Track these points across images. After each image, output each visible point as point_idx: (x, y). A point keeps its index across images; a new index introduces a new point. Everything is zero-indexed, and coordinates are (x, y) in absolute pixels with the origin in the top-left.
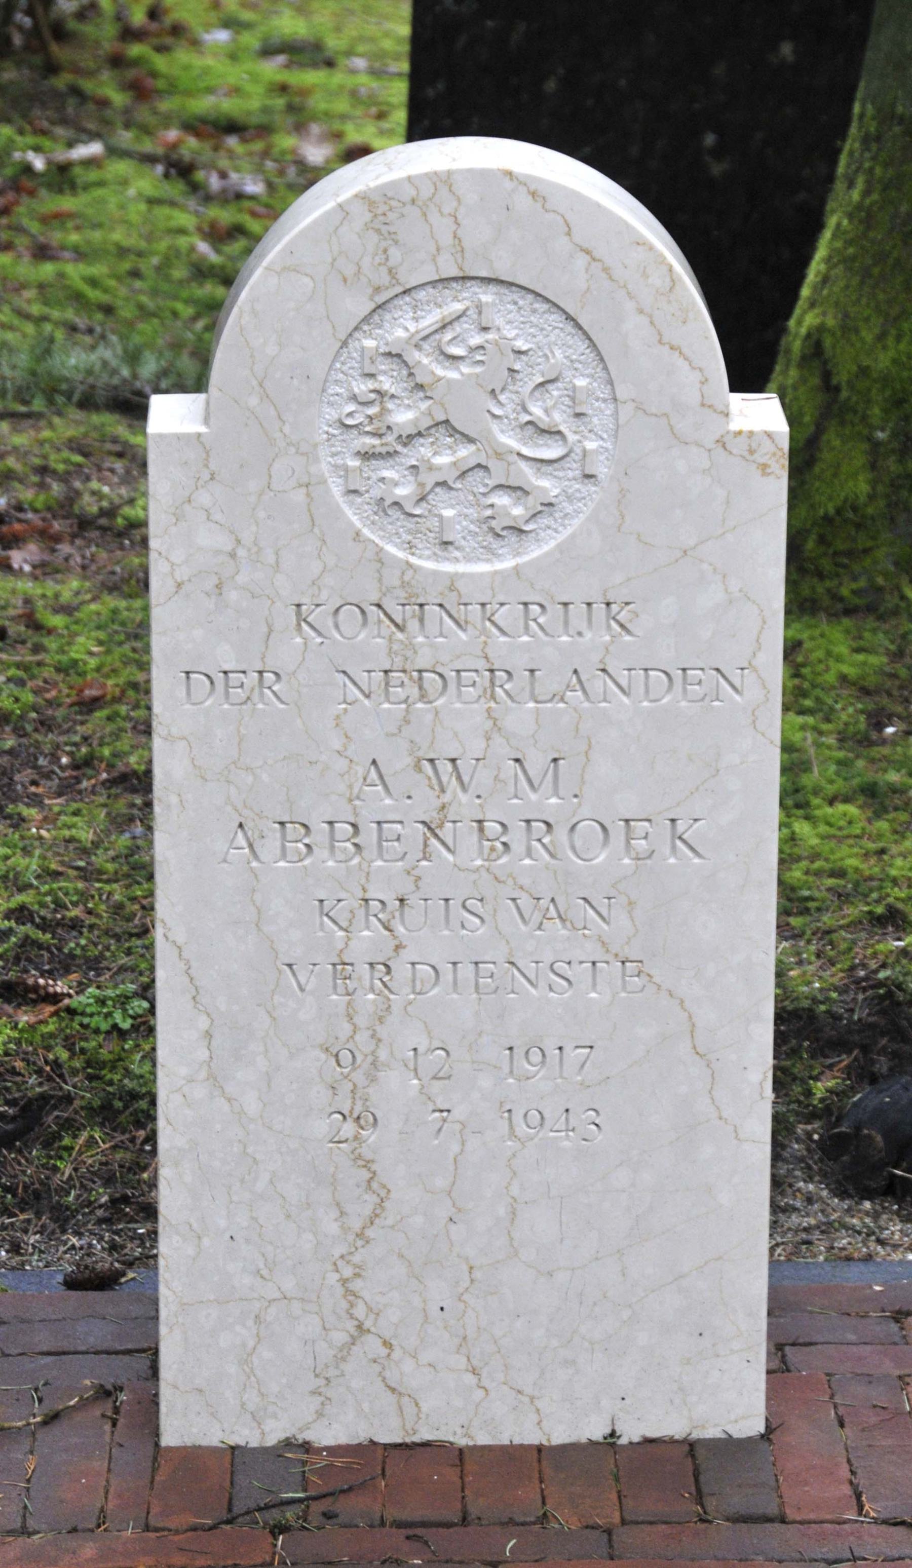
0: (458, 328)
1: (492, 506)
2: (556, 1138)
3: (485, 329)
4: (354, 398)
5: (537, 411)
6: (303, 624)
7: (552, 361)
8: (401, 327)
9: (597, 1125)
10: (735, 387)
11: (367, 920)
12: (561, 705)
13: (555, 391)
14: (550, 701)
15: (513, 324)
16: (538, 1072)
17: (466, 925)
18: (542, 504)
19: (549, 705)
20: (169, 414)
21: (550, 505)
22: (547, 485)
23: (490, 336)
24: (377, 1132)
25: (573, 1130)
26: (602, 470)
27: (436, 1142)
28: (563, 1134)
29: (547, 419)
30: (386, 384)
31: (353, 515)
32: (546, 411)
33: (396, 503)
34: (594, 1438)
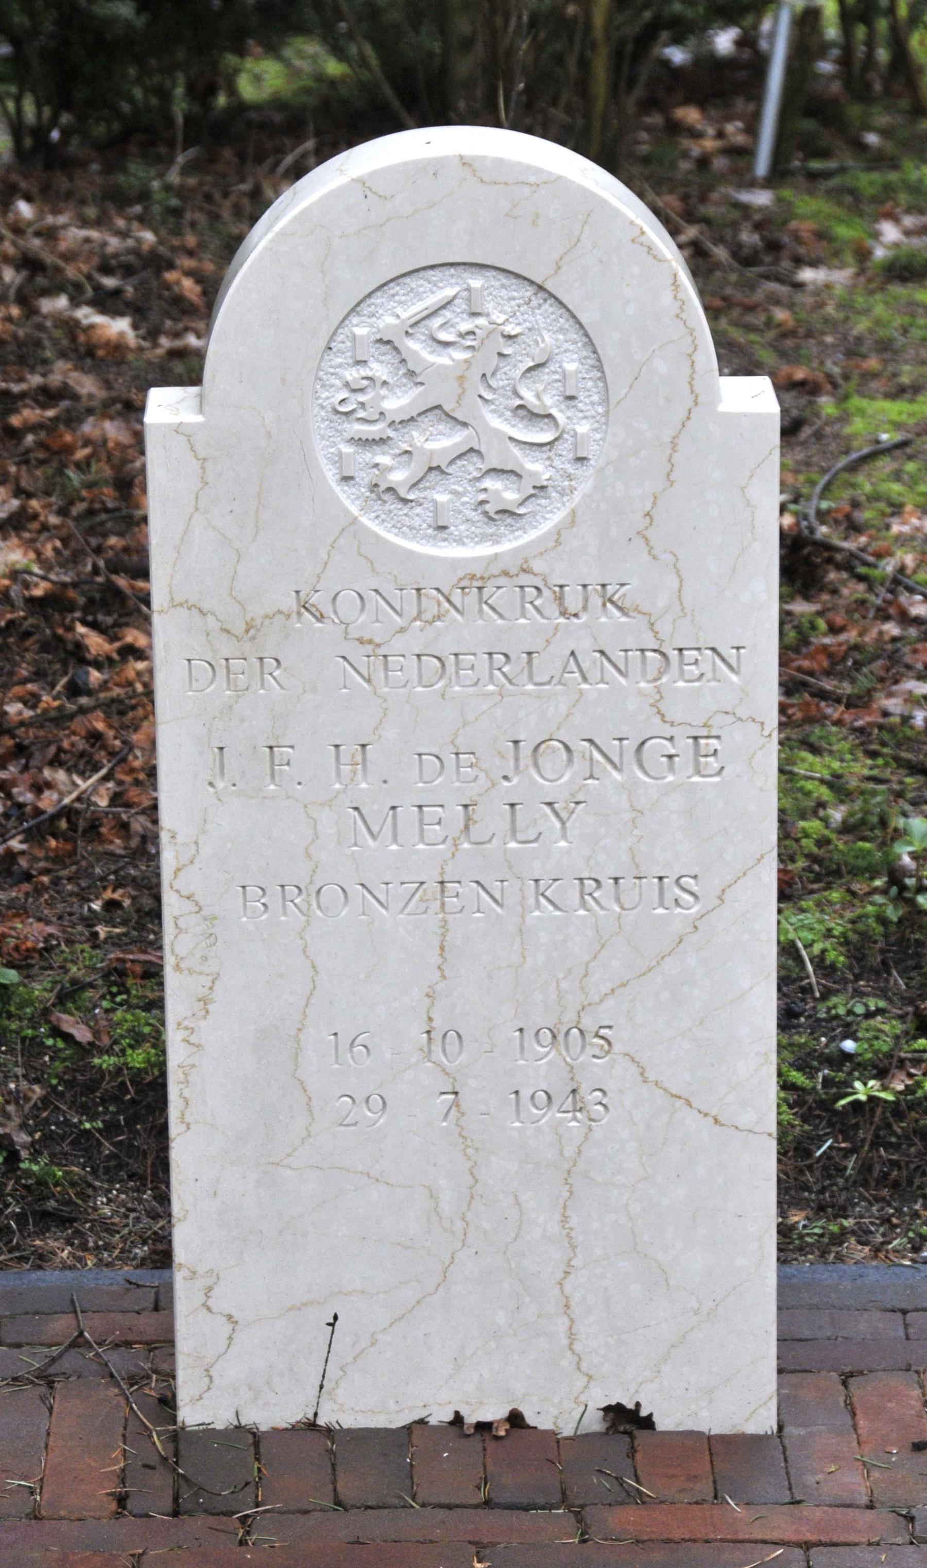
0: (447, 314)
1: (485, 490)
2: (564, 1119)
3: (475, 314)
4: (347, 385)
5: (529, 397)
6: (609, 605)
7: (542, 345)
8: (390, 315)
9: (604, 1106)
10: (721, 374)
11: (284, 906)
12: (559, 687)
13: (545, 375)
14: (549, 683)
15: (502, 307)
16: (548, 1053)
17: (681, 903)
18: (534, 487)
19: (547, 687)
20: (164, 406)
21: (543, 488)
22: (535, 467)
23: (482, 321)
24: (385, 1116)
25: (580, 1110)
26: (591, 450)
27: (445, 1124)
28: (570, 1115)
29: (536, 402)
30: (378, 370)
31: (349, 500)
32: (538, 396)
33: (390, 489)
34: (539, 1417)
